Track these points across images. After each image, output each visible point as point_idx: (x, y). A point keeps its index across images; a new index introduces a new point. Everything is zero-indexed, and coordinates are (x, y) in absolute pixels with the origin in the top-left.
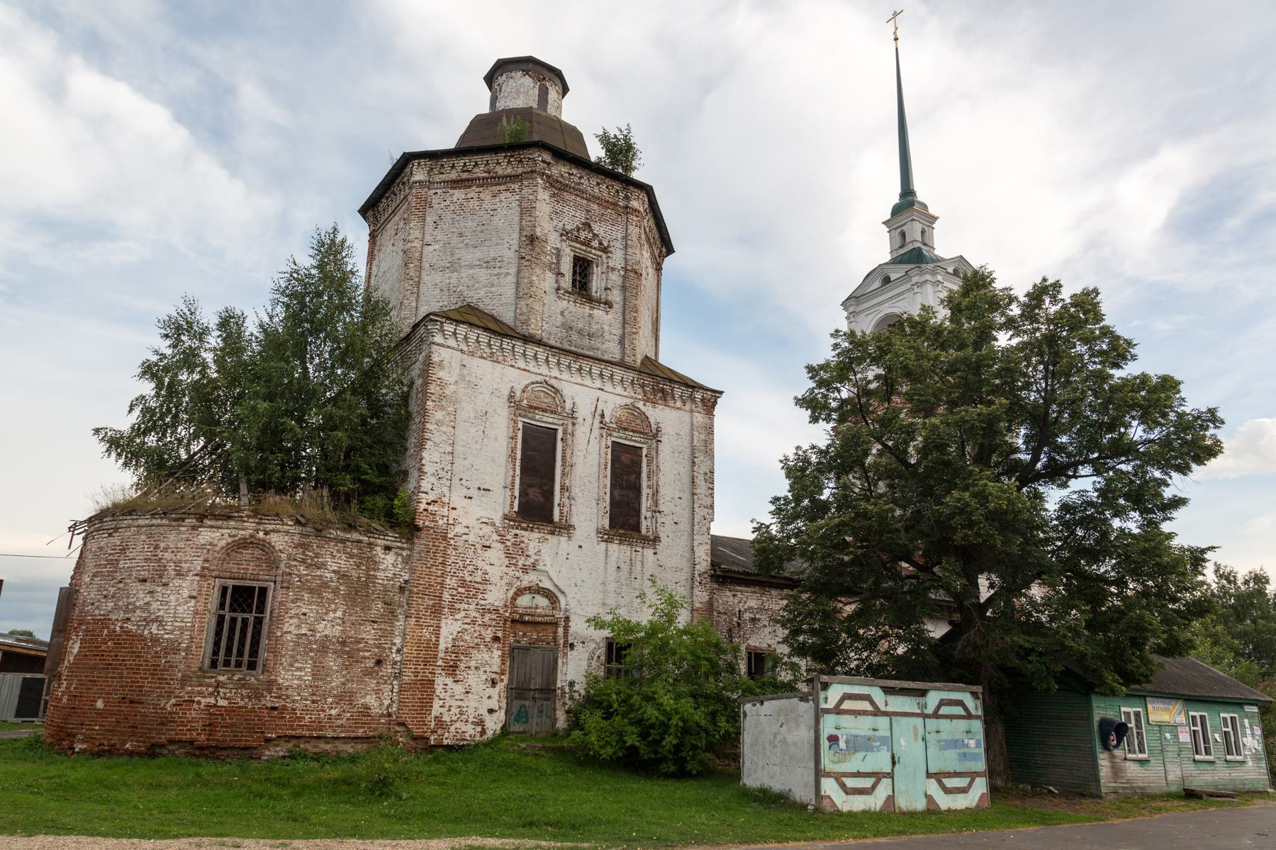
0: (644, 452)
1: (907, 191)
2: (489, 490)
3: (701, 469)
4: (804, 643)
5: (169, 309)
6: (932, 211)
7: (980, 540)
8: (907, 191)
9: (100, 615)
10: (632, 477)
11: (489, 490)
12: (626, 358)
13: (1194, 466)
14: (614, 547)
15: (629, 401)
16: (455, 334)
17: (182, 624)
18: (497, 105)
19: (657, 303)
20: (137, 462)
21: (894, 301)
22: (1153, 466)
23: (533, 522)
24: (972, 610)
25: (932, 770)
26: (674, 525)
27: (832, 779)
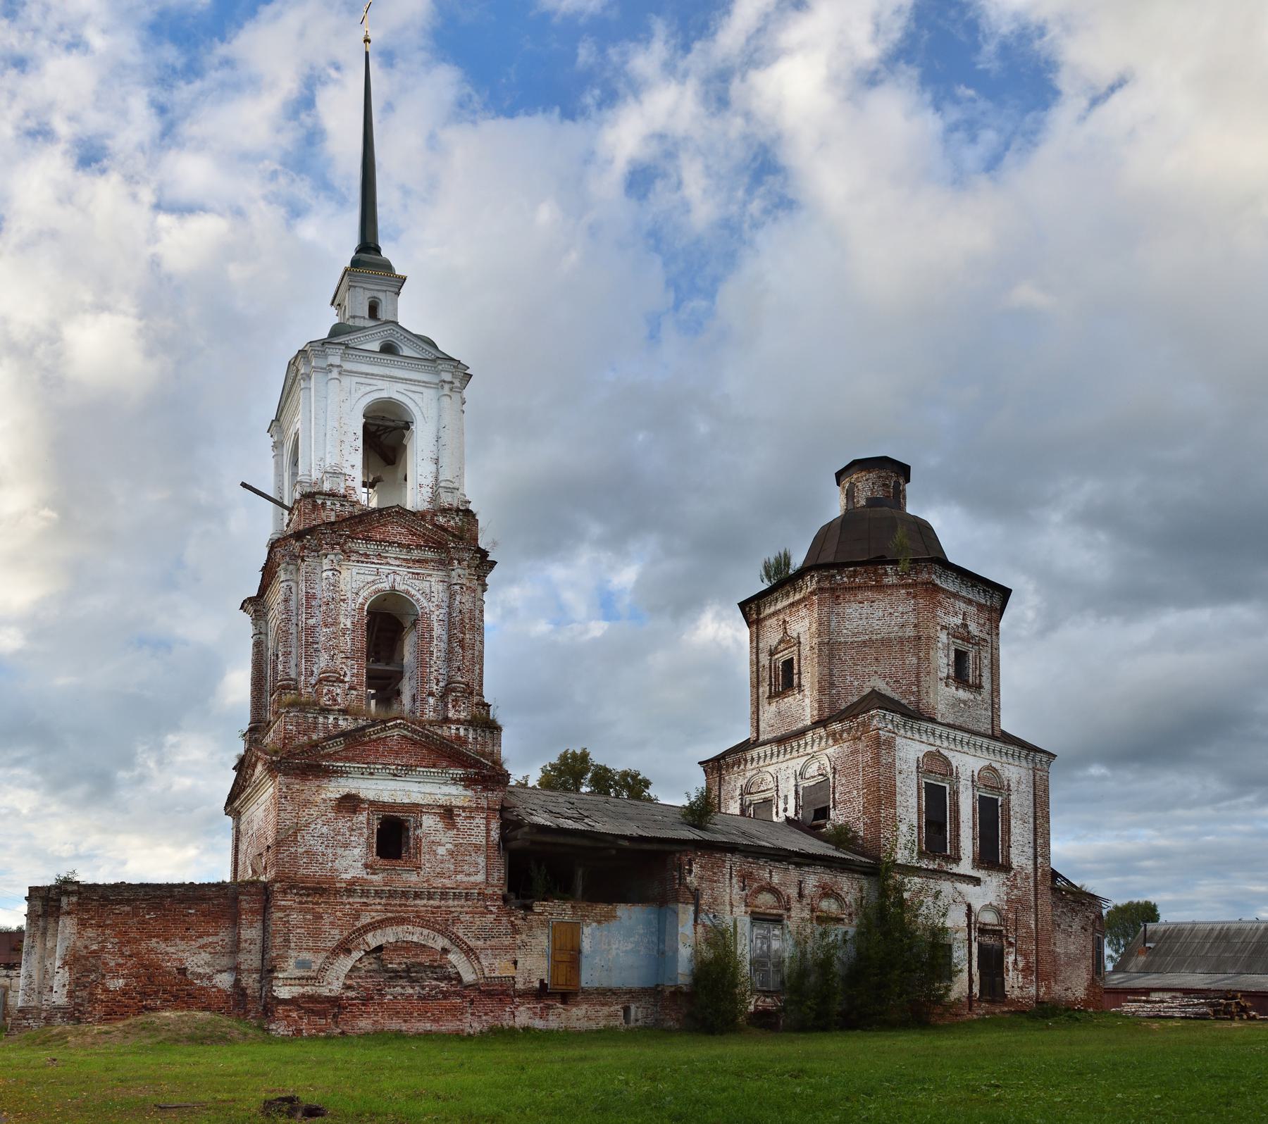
0: (971, 655)
1: (368, 245)
2: (244, 485)
3: (755, 645)
4: (1026, 971)
5: (771, 555)
6: (399, 271)
7: (1069, 1038)
8: (368, 245)
9: (428, 730)
10: (966, 678)
11: (244, 485)
12: (678, 855)
13: (970, 14)
14: (384, 479)
15: (987, 763)
16: (892, 721)
17: (351, 900)
18: (370, 935)
19: (343, 277)
20: (655, 800)
21: (414, 388)
22: (371, 711)
23: (404, 840)
24: (780, 669)
25: (308, 390)
26: (353, 464)
27: (1001, 728)
